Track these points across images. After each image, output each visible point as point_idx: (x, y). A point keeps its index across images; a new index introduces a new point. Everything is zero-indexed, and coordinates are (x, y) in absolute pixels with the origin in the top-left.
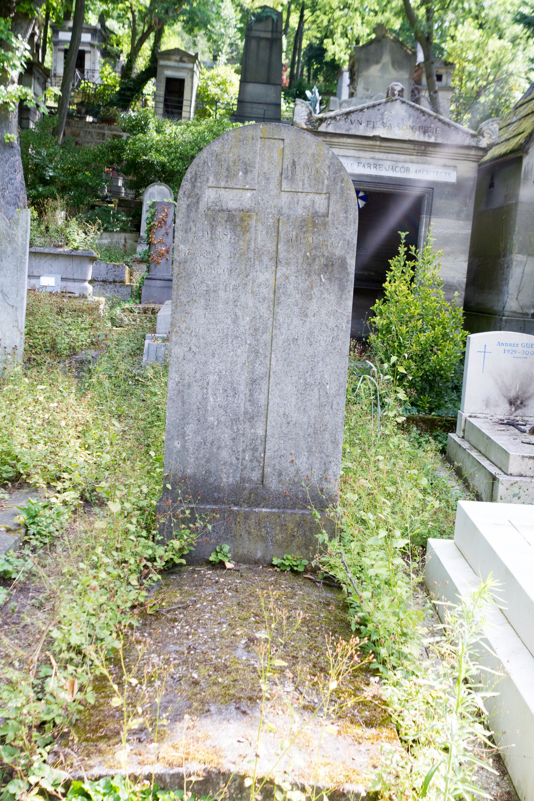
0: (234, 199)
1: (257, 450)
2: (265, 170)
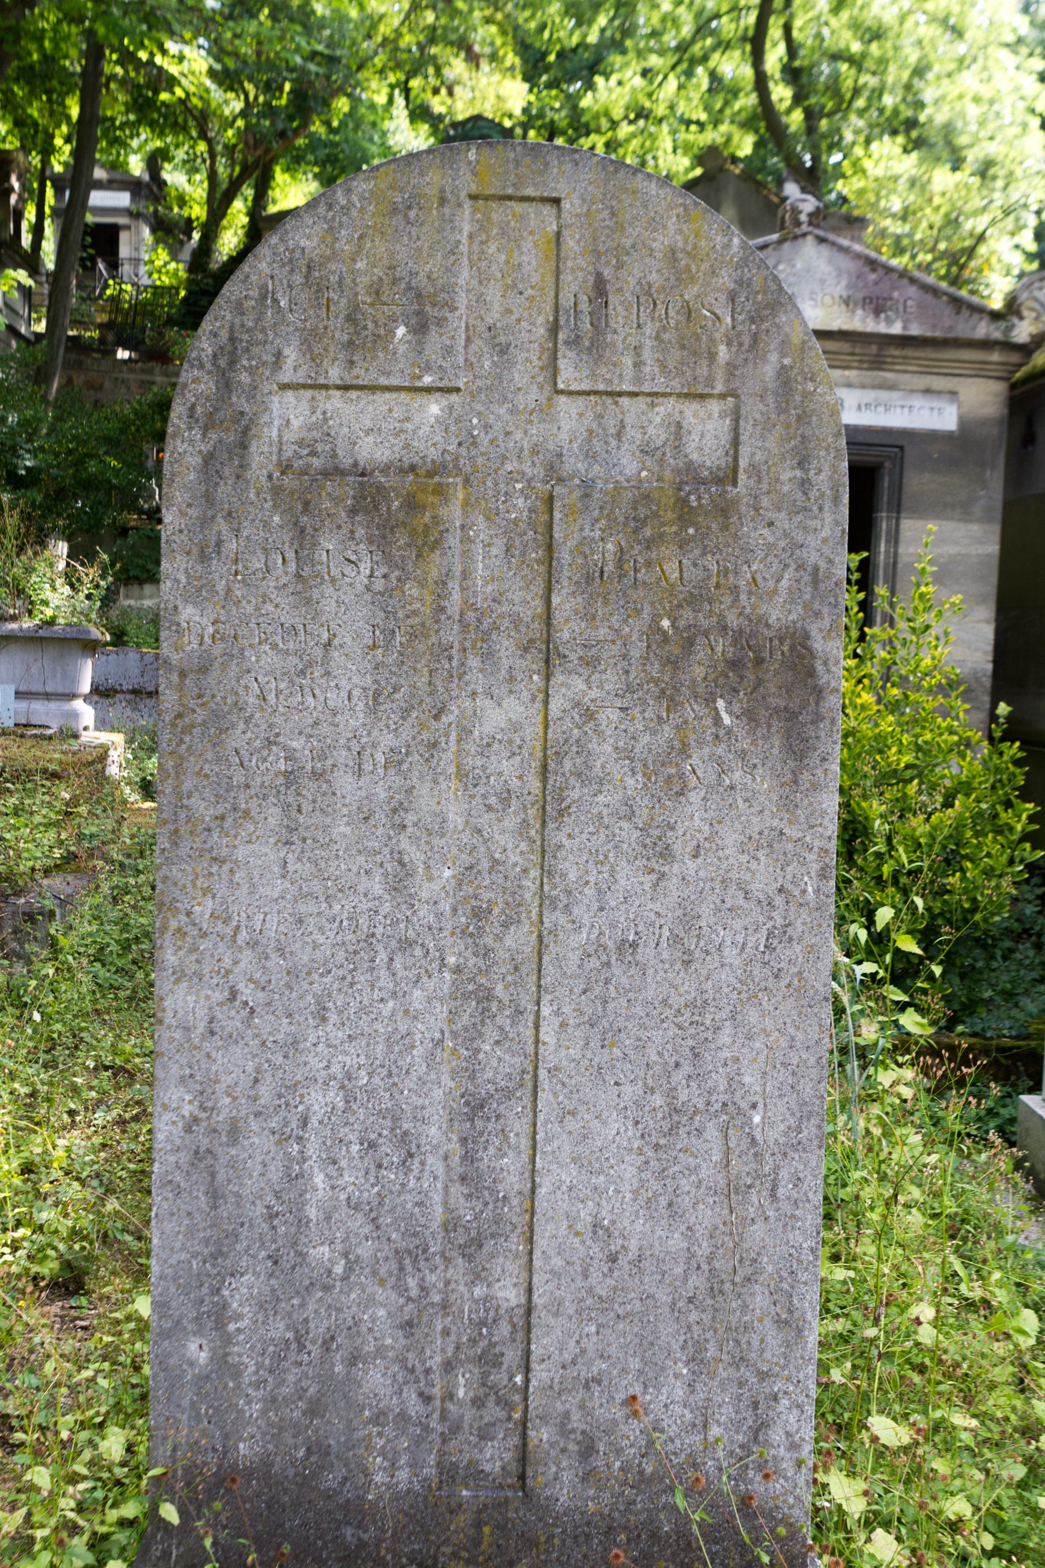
0: (375, 429)
1: (496, 1363)
2: (493, 316)
